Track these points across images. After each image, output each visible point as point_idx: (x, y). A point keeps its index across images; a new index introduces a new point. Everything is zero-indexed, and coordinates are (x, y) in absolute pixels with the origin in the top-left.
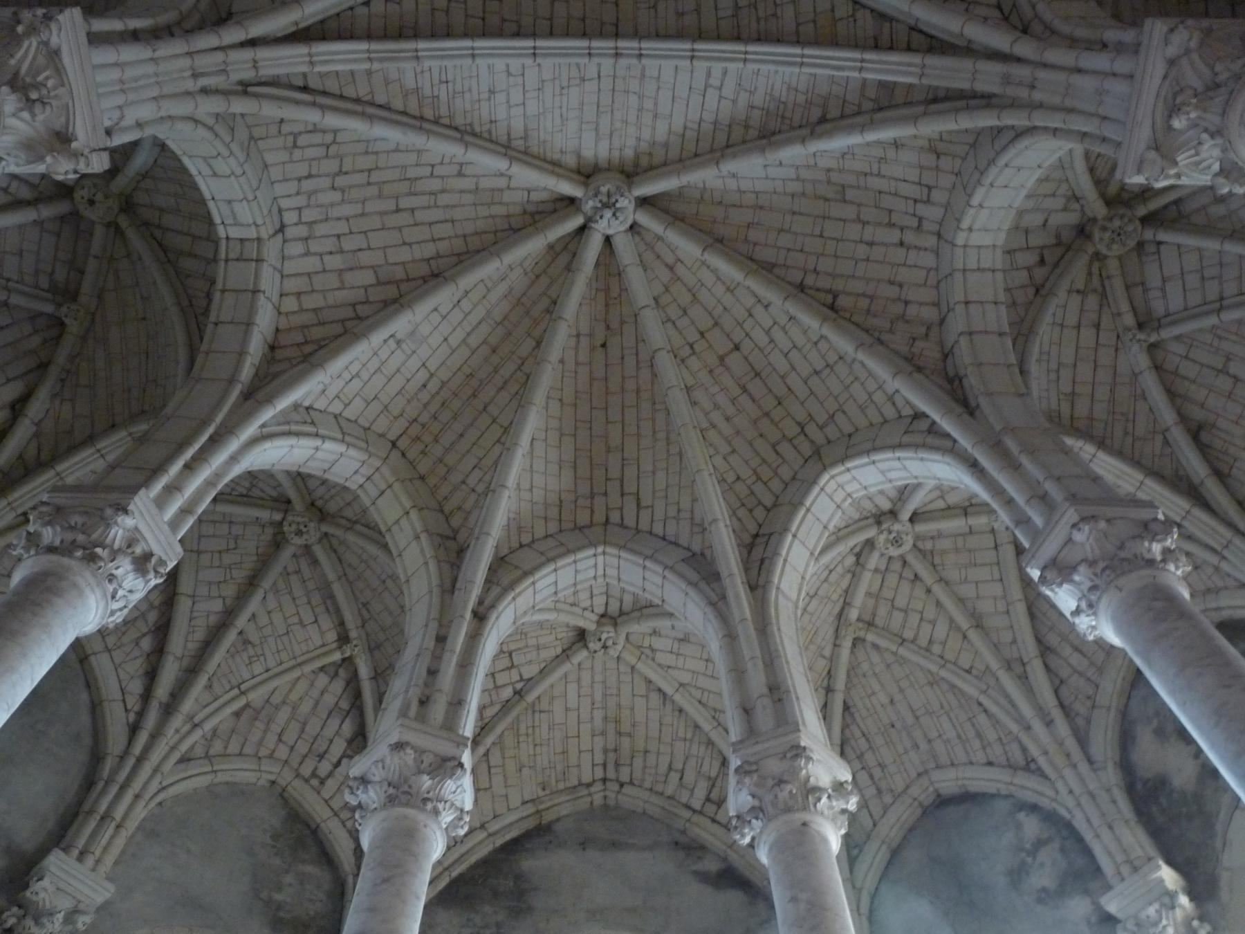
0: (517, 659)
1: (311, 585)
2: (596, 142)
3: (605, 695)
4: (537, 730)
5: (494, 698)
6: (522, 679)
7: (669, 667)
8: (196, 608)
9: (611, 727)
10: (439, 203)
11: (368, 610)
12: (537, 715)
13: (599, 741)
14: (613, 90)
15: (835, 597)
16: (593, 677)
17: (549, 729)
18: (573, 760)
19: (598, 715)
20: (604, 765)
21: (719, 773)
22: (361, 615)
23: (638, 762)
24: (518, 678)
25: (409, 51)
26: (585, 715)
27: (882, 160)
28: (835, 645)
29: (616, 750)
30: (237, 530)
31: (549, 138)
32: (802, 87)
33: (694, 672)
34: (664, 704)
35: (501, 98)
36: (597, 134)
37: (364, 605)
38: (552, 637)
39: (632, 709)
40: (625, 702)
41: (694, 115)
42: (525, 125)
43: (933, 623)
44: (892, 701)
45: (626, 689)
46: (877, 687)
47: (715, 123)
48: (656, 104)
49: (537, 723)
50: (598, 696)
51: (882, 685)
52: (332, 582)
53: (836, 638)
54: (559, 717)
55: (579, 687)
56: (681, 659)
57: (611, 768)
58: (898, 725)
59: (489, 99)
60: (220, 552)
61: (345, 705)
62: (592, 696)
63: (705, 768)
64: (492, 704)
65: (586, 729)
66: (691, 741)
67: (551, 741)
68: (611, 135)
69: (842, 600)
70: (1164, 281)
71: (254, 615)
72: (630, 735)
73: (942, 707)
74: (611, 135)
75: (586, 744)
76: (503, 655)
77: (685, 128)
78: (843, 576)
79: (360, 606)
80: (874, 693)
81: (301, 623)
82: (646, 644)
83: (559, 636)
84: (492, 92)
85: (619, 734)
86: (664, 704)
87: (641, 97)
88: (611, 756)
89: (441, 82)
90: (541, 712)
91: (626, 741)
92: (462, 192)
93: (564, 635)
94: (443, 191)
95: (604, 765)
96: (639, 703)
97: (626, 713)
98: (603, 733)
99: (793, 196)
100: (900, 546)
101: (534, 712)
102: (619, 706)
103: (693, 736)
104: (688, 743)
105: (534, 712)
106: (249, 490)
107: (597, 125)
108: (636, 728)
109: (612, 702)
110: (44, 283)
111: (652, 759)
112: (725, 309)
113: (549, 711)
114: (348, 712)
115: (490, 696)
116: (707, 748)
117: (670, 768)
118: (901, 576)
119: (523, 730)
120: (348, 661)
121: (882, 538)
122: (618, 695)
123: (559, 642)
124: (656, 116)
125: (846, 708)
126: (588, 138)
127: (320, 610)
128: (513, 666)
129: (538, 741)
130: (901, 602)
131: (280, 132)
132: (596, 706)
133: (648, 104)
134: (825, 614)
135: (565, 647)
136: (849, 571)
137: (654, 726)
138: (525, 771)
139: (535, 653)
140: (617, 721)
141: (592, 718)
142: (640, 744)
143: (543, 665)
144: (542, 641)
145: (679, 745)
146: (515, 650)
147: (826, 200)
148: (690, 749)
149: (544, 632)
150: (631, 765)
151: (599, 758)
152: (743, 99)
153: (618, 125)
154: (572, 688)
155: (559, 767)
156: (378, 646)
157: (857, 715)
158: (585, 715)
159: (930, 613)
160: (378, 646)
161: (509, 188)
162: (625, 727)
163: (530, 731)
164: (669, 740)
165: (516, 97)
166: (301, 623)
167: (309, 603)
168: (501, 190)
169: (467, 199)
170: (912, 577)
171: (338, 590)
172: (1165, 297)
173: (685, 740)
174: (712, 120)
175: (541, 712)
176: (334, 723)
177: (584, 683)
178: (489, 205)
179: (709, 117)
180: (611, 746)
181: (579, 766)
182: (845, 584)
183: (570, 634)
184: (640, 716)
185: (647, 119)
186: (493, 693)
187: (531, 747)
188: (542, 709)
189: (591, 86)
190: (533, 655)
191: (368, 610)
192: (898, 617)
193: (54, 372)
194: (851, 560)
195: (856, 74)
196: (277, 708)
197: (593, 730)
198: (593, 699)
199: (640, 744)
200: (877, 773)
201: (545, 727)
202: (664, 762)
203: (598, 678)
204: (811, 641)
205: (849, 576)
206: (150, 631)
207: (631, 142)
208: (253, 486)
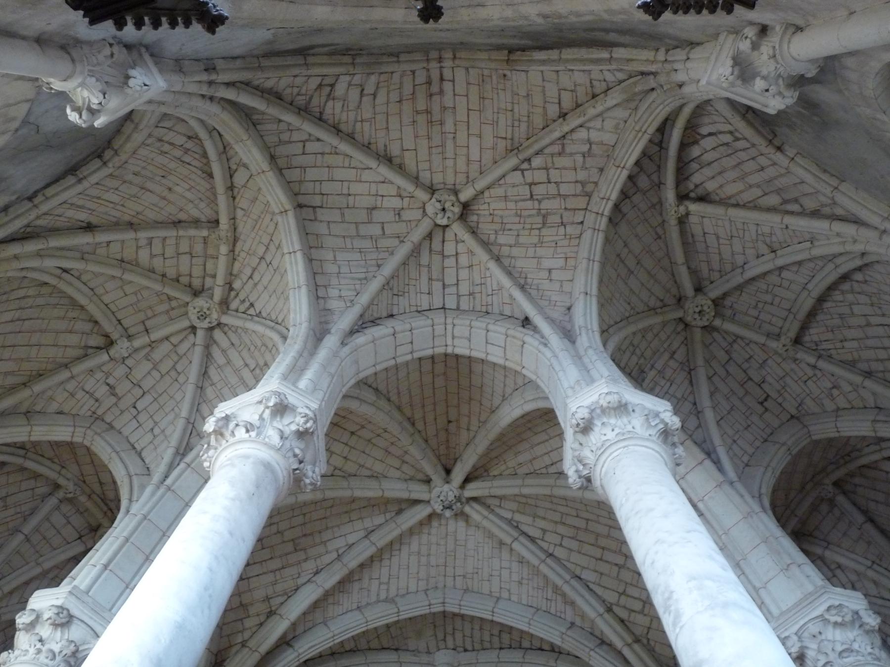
0: (526, 191)
1: (702, 257)
2: (456, 532)
3: (443, 146)
4: (509, 123)
5: (549, 160)
6: (523, 171)
7: (383, 182)
8: (806, 281)
9: (436, 117)
10: (559, 514)
11: (657, 233)
12: (509, 136)
13: (448, 101)
14: (446, 566)
15: (243, 255)
16: (455, 164)
17: (497, 122)
18: (474, 90)
19: (449, 127)
20: (442, 79)
21: (325, 105)
22: (664, 229)
23: (408, 89)
24: (526, 173)
25: (591, 324)
26: (462, 128)
27: (275, 583)
28: (234, 218)
29: (431, 95)
30: (754, 313)
31: (487, 540)
32: (331, 607)
33: (361, 181)
34: (385, 146)
35: (515, 577)
36: (455, 537)
37: (660, 237)
38: (493, 206)
39: (416, 137)
40: (424, 143)
41: (395, 560)
42: (501, 552)
43: (152, 256)
44: (170, 189)
45: (423, 154)
46: (188, 195)
47: (381, 560)
48: (419, 562)
49: (510, 129)
50: (450, 145)
51: (184, 197)
52: (683, 264)
53: (234, 224)
54: (488, 130)
55: (468, 156)
56: (373, 192)
57: (435, 75)
58: (158, 178)
59: (522, 578)
60: (772, 304)
61: (694, 166)
62: (456, 146)
63: (338, 105)
64: (552, 155)
65: (462, 115)
66: (356, 121)
67: (496, 110)
68: (447, 535)
69: (236, 253)
70: (69, 523)
71: (758, 257)
72: (418, 112)
73: (123, 205)
74: (447, 535)
75: (462, 103)
76: (539, 197)
77: (400, 550)
78: (240, 272)
79: (663, 236)
80: (189, 190)
81: (718, 238)
82: (406, 200)
83: (486, 206)
84: (520, 583)
85: (428, 112)
86: (385, 146)
87: (428, 564)
88: (435, 88)
89: (551, 600)
90: (505, 138)
91: (421, 105)
92: (544, 518)
93: (482, 207)
94: (556, 523)
95: (442, 79)
96: (409, 144)
97: (422, 132)
98: (444, 109)
99: (327, 528)
100: (199, 318)
101: (512, 139)
102: (429, 138)
103: (354, 126)
104: (359, 119)
105: (512, 139)
106: (735, 341)
107: (455, 544)
108: (411, 120)
109: (437, 140)
110: (836, 512)
111: (395, 97)
112: (364, 452)
113: (497, 137)
114: (693, 160)
115: (553, 162)
116: (340, 120)
117: (375, 95)
118: (190, 276)
119: (524, 126)
120: (682, 197)
121: (215, 316)
122: (431, 148)
123: (487, 200)
124: (419, 553)
125: (211, 176)
126: (461, 536)
127: (700, 247)
128: (530, 185)
129: (509, 114)
130: (185, 259)
131: (652, 620)
132: (452, 136)
133: (424, 560)
134: (249, 242)
135: (481, 196)
136: (236, 276)
137: (394, 122)
138: (523, 93)
139: (509, 194)
140: (430, 122)
141: (455, 125)
142: (407, 107)
143: (502, 182)
144: (502, 205)
145: (367, 115)
146: (527, 200)
147: (305, 535)
148: (357, 114)
149: (500, 213)
150: (414, 86)
151: (448, 86)
152: (366, 581)
153: (442, 542)
154: (475, 155)
155: (488, 87)
156: (653, 206)
157: (199, 173)
158: (462, 128)
159: (157, 263)
160: (653, 206)
161: (514, 512)
162: (422, 119)
163: (516, 124)
164: (378, 117)
165: (506, 574)
166: (718, 238)
167: (707, 247)
168: (518, 511)
169: (541, 513)
170: (181, 279)
171: (679, 255)
172: (64, 515)
173: (362, 121)
174: (383, 562)
175: (505, 138)
176: (708, 157)
177: (464, 159)
178: (526, 504)
179: (386, 562)
180: (436, 98)
181: (468, 84)
182: (237, 265)
183: (476, 207)
184: (408, 131)
185: (424, 550)
186: (550, 165)
187: (516, 110)
188: (504, 141)
189: (459, 571)
190: (511, 192)
191: (657, 233)
192: (184, 247)
193: (852, 466)
194: (237, 285)
195: (301, 651)
196: (758, 186)
197: (454, 113)
198: (455, 143)
199: (407, 107)
200: (167, 147)
201: (502, 122)
202: (381, 98)
203: (449, 163)
204: (257, 221)
205: (235, 272)
206: (852, 280)
207: (434, 531)
208: (731, 344)
